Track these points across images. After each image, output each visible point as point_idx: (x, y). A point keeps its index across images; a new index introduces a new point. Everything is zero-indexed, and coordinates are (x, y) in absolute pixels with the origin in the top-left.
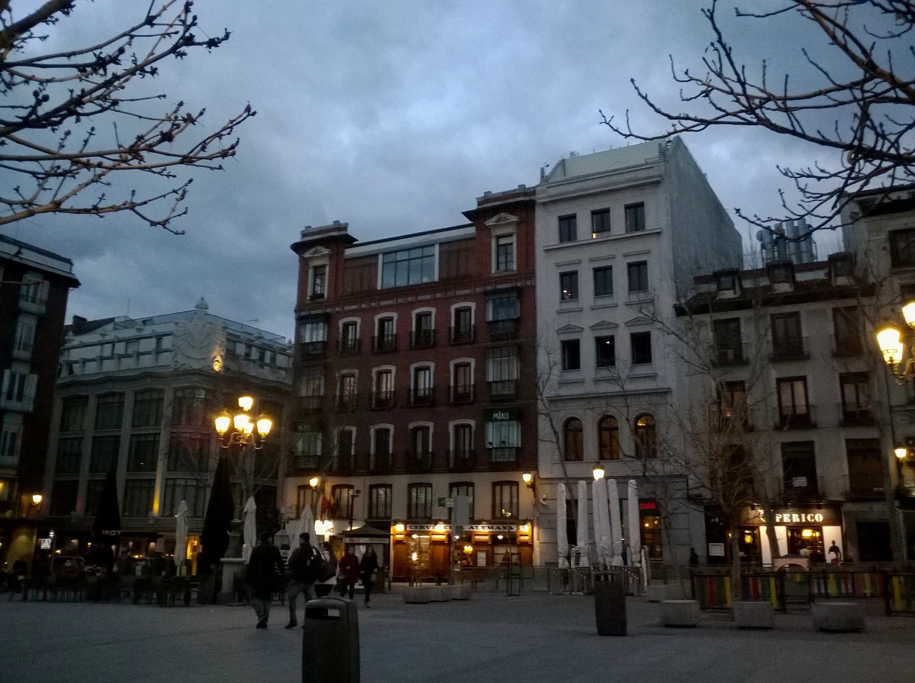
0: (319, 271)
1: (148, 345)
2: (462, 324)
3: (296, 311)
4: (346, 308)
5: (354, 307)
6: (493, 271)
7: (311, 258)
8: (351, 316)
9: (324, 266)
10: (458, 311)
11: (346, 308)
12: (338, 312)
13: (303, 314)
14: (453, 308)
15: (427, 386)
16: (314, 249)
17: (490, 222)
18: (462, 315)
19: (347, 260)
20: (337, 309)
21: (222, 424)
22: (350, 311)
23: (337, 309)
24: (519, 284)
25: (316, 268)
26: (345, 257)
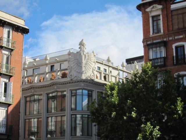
0: (155, 19)
1: (48, 69)
2: (179, 54)
3: (143, 42)
4: (176, 38)
5: (181, 36)
6: (151, 34)
7: (151, 11)
8: (179, 42)
9: (159, 15)
10: (177, 48)
11: (176, 38)
12: (171, 40)
13: (149, 43)
14: (174, 46)
15: (4, 123)
16: (152, 7)
17: (148, 10)
18: (179, 49)
19: (172, 11)
20: (171, 39)
21: (127, 113)
22: (178, 39)
23: (171, 39)
24: (165, 40)
25: (153, 17)
26: (171, 10)
